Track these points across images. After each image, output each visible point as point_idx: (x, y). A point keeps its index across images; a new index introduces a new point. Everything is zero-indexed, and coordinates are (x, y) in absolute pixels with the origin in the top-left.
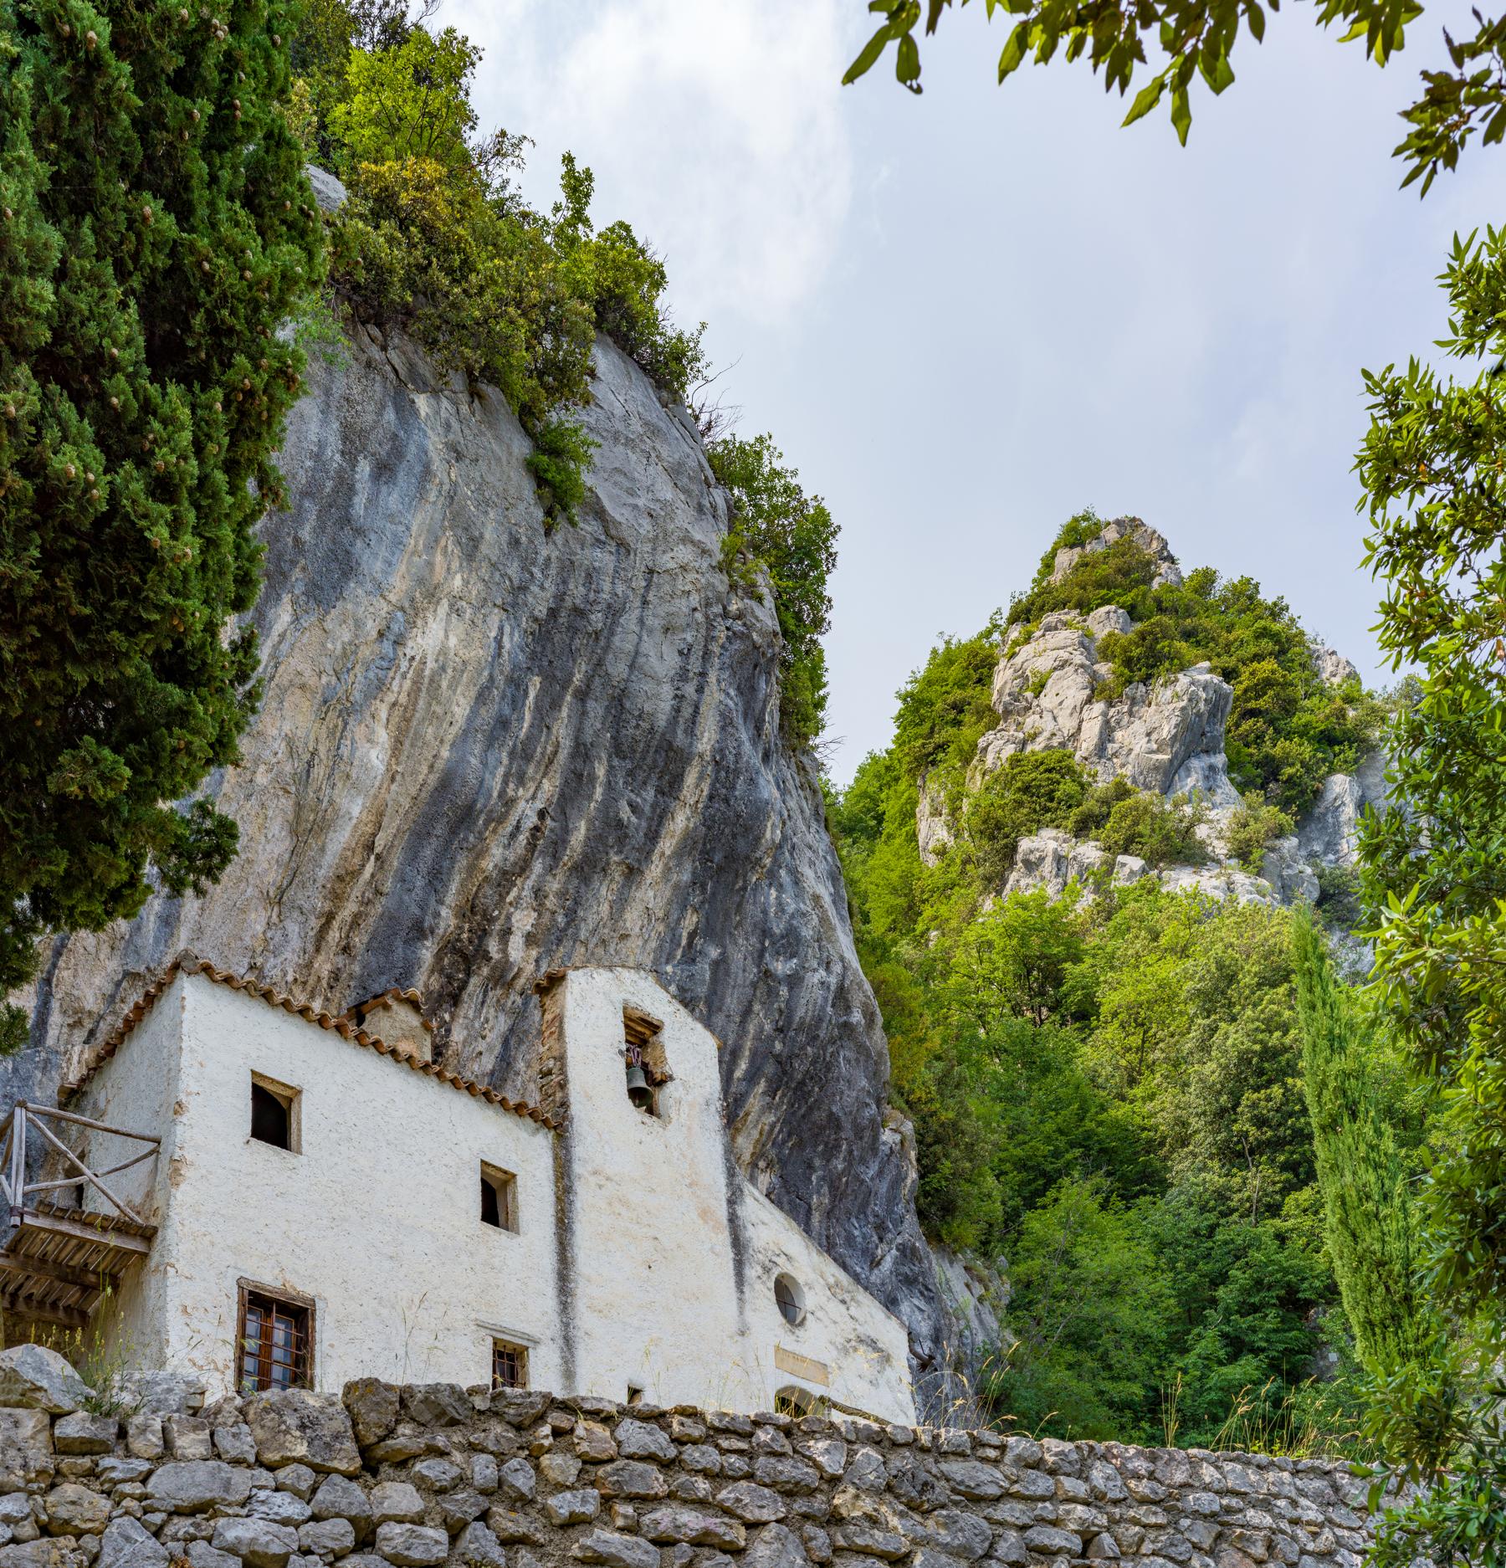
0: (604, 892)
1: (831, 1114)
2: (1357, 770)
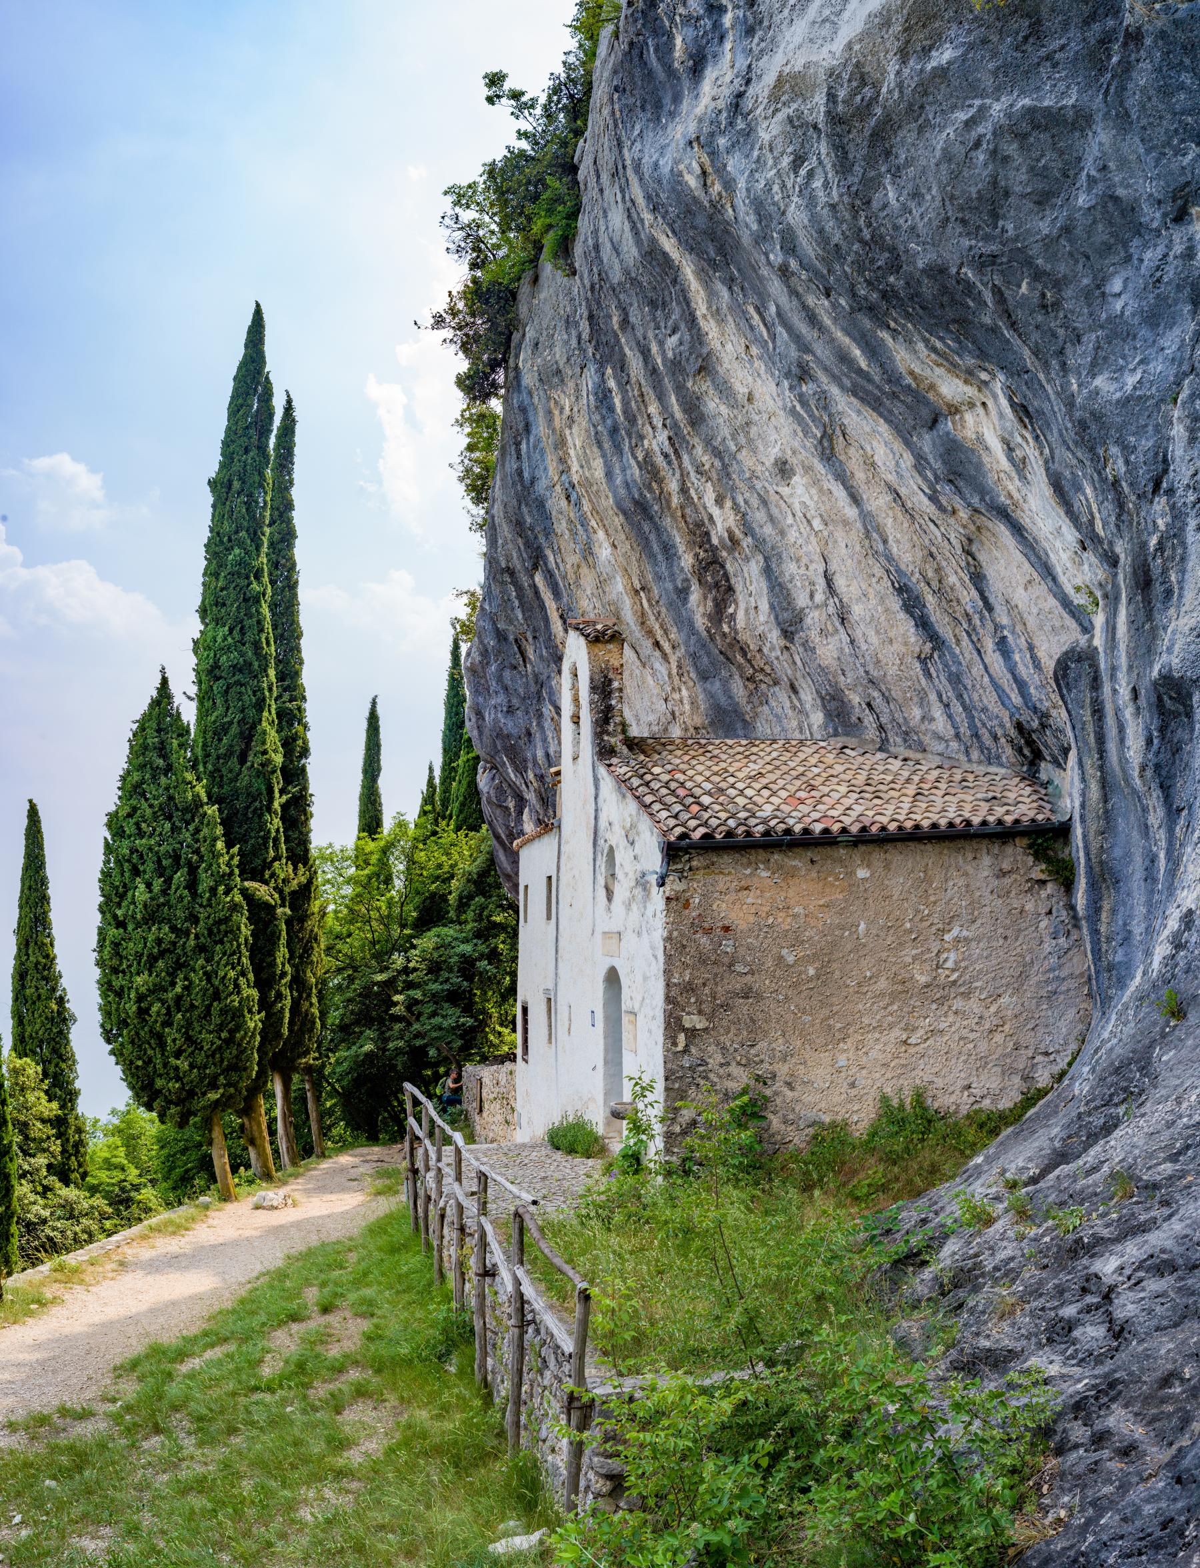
0: (713, 405)
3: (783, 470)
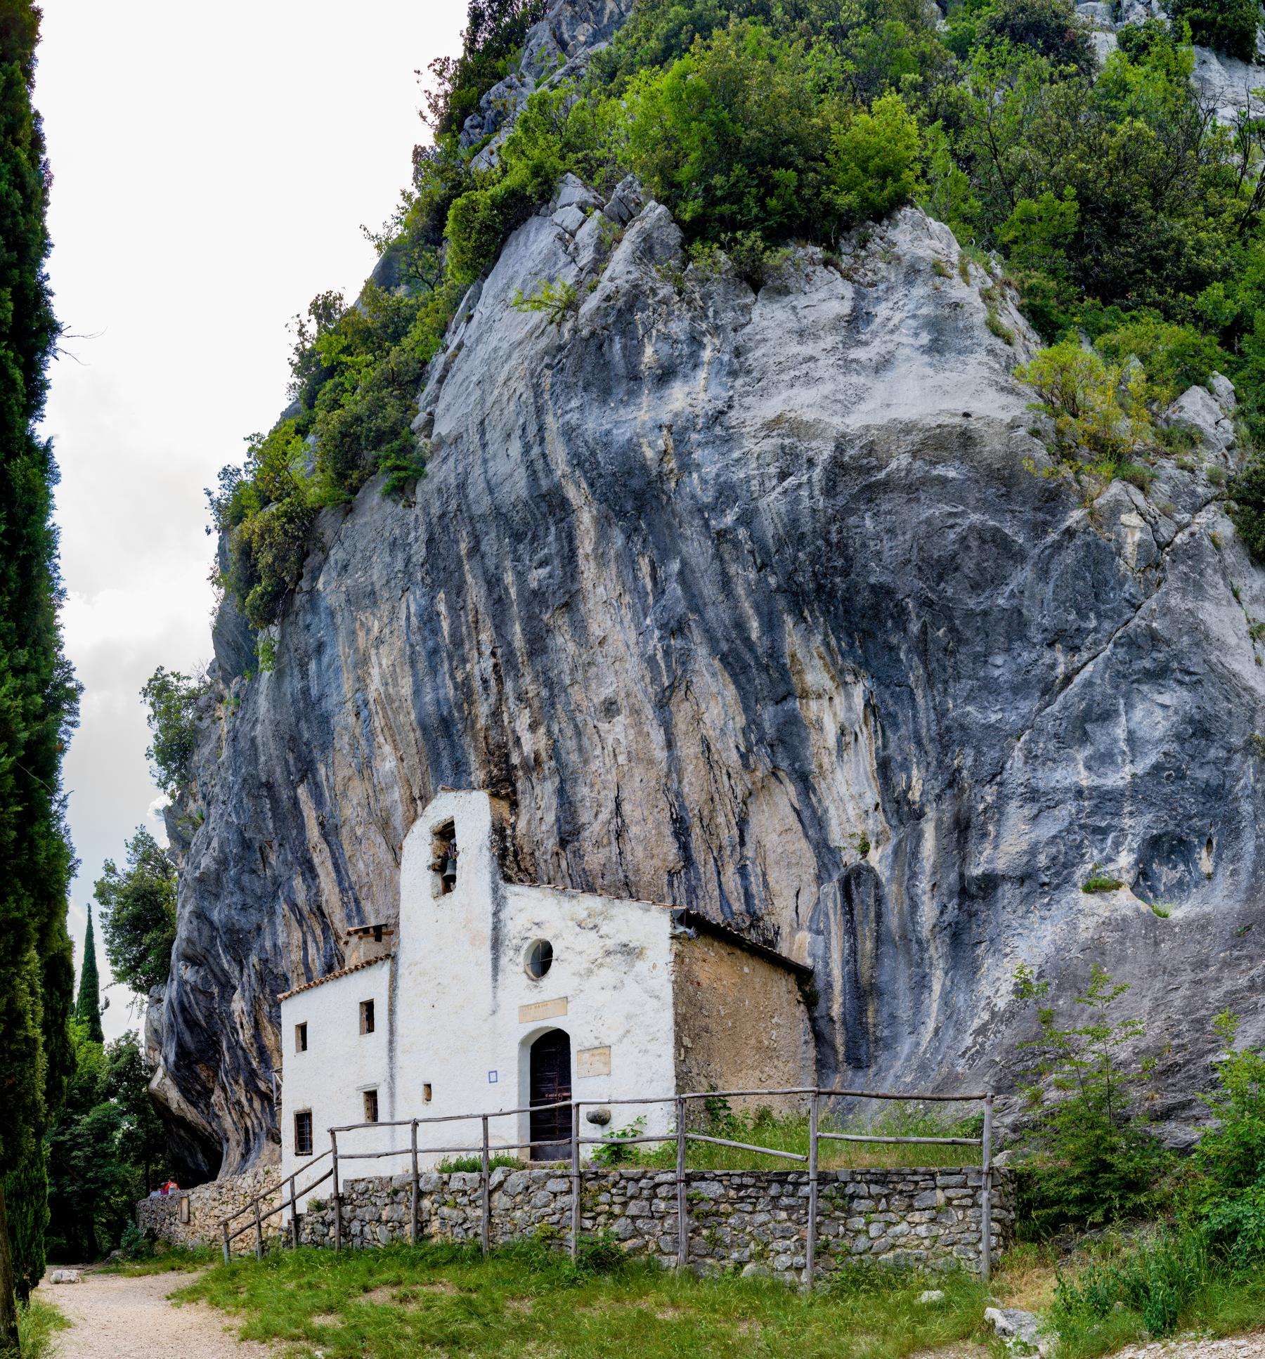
0: (564, 642)
1: (873, 587)
3: (610, 709)
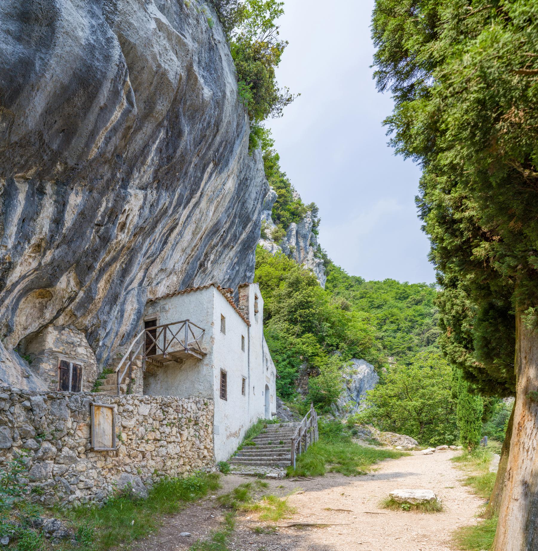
2: (297, 223)
